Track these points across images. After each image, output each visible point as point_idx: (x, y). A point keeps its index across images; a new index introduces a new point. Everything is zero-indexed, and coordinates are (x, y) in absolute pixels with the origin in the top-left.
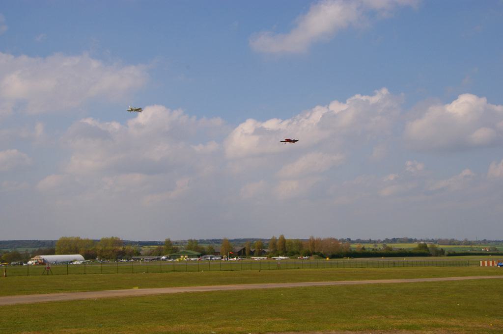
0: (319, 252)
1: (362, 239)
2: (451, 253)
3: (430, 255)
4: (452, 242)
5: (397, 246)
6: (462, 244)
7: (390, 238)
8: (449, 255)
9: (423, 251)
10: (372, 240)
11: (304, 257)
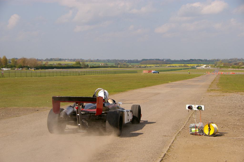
0: (27, 66)
1: (92, 59)
2: (91, 66)
3: (82, 68)
4: (98, 61)
5: (50, 63)
6: (88, 62)
7: (49, 58)
8: (91, 68)
9: (78, 65)
10: (39, 59)
11: (19, 69)
